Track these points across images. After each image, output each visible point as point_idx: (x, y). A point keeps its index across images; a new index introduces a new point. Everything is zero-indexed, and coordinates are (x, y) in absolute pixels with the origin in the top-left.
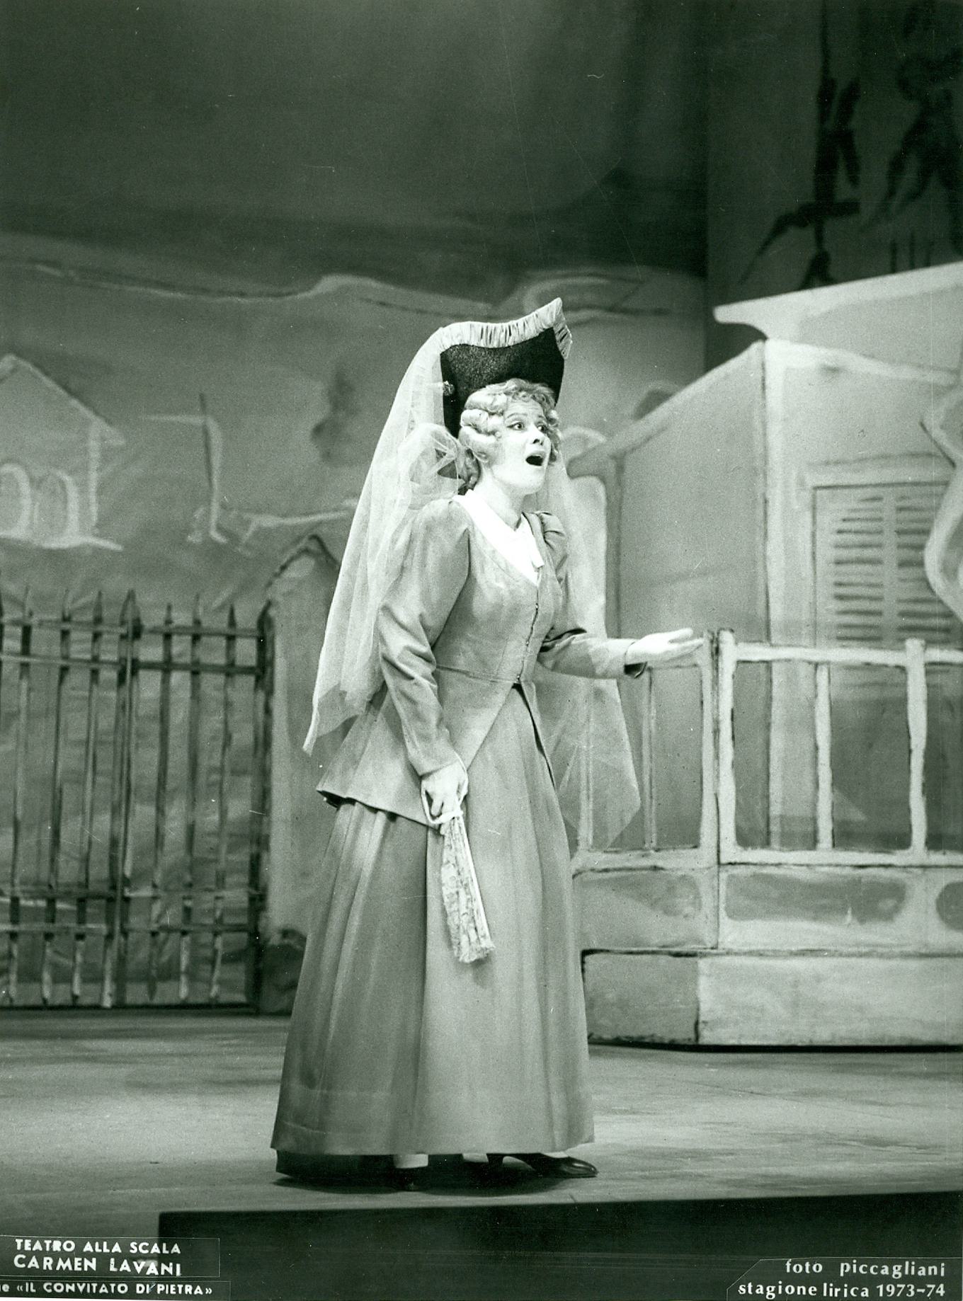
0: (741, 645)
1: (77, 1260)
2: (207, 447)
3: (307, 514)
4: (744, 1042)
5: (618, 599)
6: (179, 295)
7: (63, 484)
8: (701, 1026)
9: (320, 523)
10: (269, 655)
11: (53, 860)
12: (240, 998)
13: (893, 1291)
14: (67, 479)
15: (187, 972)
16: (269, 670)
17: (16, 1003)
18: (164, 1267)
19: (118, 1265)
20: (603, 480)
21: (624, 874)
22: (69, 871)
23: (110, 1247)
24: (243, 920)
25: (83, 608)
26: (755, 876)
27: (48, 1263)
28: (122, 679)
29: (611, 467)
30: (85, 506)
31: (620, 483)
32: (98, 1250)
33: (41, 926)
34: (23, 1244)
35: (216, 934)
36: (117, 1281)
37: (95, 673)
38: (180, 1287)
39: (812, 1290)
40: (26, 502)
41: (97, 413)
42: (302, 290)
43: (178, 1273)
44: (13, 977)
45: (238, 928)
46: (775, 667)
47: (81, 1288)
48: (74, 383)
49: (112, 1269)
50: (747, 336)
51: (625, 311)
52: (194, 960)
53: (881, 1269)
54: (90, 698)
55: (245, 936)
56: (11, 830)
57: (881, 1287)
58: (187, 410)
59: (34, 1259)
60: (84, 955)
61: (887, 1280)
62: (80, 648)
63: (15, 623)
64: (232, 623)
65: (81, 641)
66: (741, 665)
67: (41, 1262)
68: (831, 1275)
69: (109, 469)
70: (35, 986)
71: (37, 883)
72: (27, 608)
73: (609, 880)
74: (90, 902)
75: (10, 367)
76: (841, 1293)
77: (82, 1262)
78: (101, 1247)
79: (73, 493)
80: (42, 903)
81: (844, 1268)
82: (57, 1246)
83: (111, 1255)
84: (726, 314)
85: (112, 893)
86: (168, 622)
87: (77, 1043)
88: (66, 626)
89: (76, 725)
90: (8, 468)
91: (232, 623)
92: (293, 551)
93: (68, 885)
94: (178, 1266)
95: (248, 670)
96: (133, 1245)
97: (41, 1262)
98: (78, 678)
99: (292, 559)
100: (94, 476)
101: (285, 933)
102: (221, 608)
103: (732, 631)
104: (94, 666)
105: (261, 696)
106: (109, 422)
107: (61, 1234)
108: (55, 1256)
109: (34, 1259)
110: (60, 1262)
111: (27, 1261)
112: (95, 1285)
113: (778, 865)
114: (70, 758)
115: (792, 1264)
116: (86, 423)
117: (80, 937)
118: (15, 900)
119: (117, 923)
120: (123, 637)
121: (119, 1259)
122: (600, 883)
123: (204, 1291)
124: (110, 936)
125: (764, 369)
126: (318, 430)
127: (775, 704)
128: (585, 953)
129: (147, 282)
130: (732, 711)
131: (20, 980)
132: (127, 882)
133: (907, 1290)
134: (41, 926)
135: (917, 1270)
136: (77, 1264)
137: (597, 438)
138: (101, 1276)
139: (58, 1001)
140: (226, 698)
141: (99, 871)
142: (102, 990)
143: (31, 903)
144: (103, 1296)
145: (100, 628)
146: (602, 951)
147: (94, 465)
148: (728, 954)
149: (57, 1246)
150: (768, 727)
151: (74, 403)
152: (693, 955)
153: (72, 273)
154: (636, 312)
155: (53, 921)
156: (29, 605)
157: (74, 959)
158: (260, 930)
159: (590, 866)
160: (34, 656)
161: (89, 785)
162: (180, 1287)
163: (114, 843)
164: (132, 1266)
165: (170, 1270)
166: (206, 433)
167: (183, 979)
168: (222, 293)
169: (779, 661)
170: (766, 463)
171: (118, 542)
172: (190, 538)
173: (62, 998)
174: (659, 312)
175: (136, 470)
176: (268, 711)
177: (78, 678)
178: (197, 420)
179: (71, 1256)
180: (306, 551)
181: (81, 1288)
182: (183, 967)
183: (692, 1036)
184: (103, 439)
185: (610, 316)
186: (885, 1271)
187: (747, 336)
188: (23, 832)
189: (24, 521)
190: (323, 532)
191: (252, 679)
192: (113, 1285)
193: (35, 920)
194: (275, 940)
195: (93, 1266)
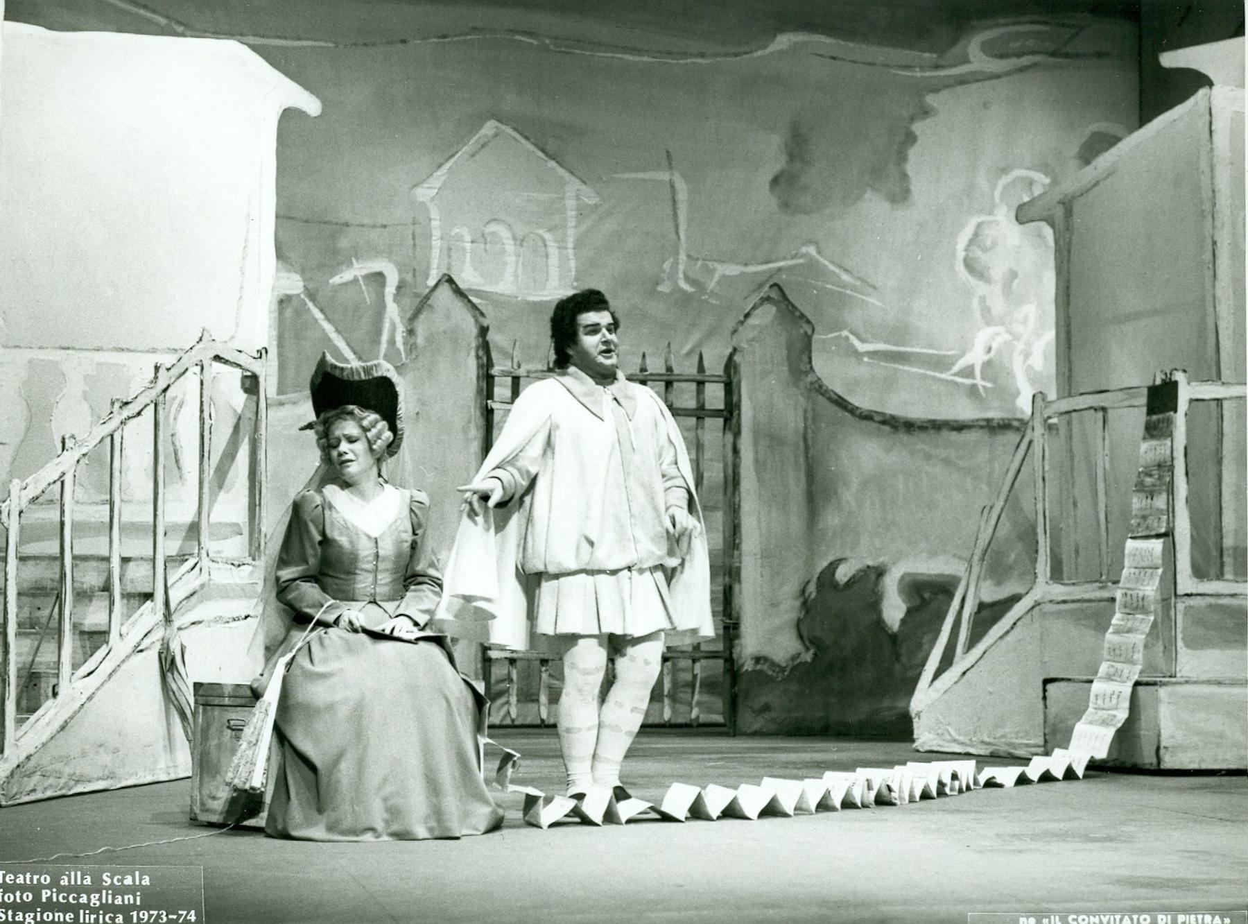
0: (1194, 384)
2: (674, 201)
3: (767, 262)
4: (1204, 767)
5: (1069, 340)
6: (645, 59)
8: (1162, 751)
9: (779, 270)
10: (735, 398)
12: (719, 719)
13: (146, 917)
14: (548, 236)
15: (669, 696)
16: (735, 414)
17: (516, 723)
20: (1052, 225)
21: (1085, 605)
24: (720, 647)
26: (1210, 606)
29: (1059, 212)
30: (563, 260)
31: (1069, 227)
35: (694, 661)
39: (69, 917)
40: (511, 259)
42: (759, 48)
44: (513, 699)
45: (713, 655)
46: (1226, 404)
48: (551, 145)
50: (1195, 81)
51: (1067, 56)
52: (675, 684)
53: (79, 897)
55: (721, 662)
57: (135, 913)
58: (657, 168)
63: (504, 374)
64: (701, 369)
66: (1194, 403)
69: (584, 227)
70: (533, 706)
72: (515, 360)
73: (1066, 611)
75: (492, 132)
76: (97, 920)
79: (553, 251)
84: (1171, 59)
86: (643, 370)
90: (492, 227)
91: (701, 369)
92: (754, 299)
95: (716, 413)
99: (754, 308)
100: (571, 234)
101: (758, 660)
102: (689, 354)
103: (1185, 371)
105: (729, 437)
113: (1233, 595)
116: (563, 183)
122: (1058, 614)
125: (1211, 114)
126: (775, 181)
127: (1226, 440)
128: (1046, 682)
129: (614, 48)
130: (1186, 449)
133: (159, 916)
135: (114, 899)
137: (1042, 179)
140: (697, 438)
146: (1063, 679)
147: (572, 223)
148: (1187, 682)
150: (1220, 461)
151: (552, 164)
152: (1155, 684)
153: (547, 41)
154: (1077, 56)
158: (735, 656)
159: (1048, 598)
166: (672, 186)
167: (666, 701)
168: (685, 55)
169: (1231, 398)
170: (1214, 205)
172: (660, 288)
174: (1100, 55)
175: (609, 226)
176: (736, 451)
178: (664, 176)
180: (767, 299)
182: (666, 693)
183: (1154, 760)
184: (578, 198)
185: (1051, 60)
186: (84, 900)
187: (1195, 81)
190: (782, 279)
191: (721, 420)
194: (749, 666)
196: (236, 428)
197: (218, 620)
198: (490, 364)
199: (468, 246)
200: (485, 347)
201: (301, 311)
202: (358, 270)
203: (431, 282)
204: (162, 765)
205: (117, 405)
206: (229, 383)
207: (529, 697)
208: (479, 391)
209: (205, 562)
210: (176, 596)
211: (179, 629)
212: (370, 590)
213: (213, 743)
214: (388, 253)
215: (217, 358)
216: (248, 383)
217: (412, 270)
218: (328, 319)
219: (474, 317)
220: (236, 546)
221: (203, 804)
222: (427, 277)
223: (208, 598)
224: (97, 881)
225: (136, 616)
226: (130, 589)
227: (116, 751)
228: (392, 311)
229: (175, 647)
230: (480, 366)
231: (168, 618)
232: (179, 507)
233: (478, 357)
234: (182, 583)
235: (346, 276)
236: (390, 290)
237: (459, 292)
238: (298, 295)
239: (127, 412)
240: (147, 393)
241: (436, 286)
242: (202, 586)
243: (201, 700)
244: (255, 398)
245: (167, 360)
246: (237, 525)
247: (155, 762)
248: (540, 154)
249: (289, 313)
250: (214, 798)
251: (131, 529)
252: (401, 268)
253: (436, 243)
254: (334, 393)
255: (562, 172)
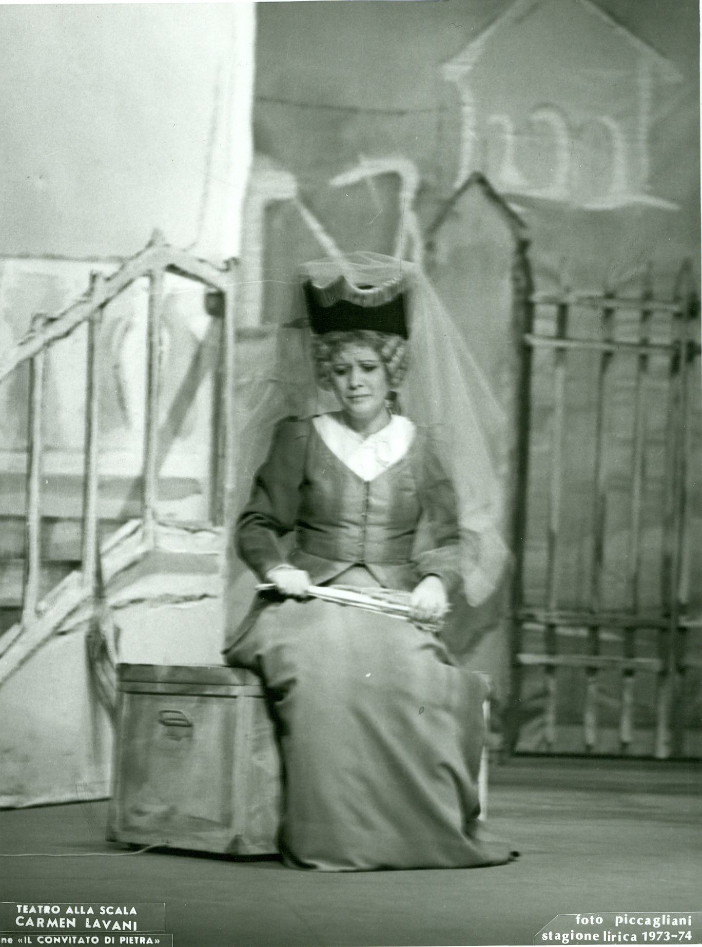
1: (61, 920)
7: (607, 135)
11: (595, 580)
14: (613, 125)
18: (124, 924)
19: (91, 923)
22: (614, 593)
23: (86, 910)
25: (631, 281)
27: (40, 922)
28: (675, 367)
32: (76, 912)
33: (581, 660)
34: (22, 908)
36: (91, 935)
37: (644, 359)
38: (136, 938)
40: (564, 155)
41: (650, 44)
43: (135, 929)
44: (550, 718)
47: (65, 940)
49: (87, 926)
54: (637, 389)
56: (545, 544)
59: (30, 920)
60: (635, 694)
61: (650, 928)
62: (626, 328)
63: (549, 301)
65: (628, 322)
67: (35, 922)
68: (608, 925)
70: (575, 730)
71: (578, 609)
74: (640, 632)
77: (65, 921)
78: (79, 910)
80: (583, 632)
81: (619, 920)
82: (47, 909)
83: (86, 916)
85: (664, 622)
87: (626, 797)
88: (610, 304)
89: (621, 418)
93: (614, 611)
94: (135, 923)
96: (102, 908)
97: (35, 922)
98: (624, 366)
100: (644, 121)
104: (643, 351)
106: (663, 54)
107: (51, 902)
108: (46, 917)
109: (30, 920)
110: (50, 922)
111: (25, 921)
112: (75, 938)
114: (614, 459)
115: (581, 917)
117: (629, 673)
118: (551, 627)
119: (672, 658)
120: (678, 316)
121: (92, 919)
123: (154, 941)
124: (663, 674)
131: (559, 722)
132: (683, 609)
134: (581, 660)
135: (671, 921)
136: (61, 923)
138: (80, 930)
139: (603, 749)
141: (650, 594)
142: (655, 736)
143: (569, 632)
144: (623, 942)
145: (650, 306)
149: (47, 909)
151: (621, 31)
155: (596, 652)
156: (566, 279)
157: (620, 698)
160: (571, 340)
161: (637, 491)
162: (136, 938)
163: (667, 562)
164: (102, 924)
165: (129, 927)
171: (673, 200)
173: (605, 742)
177: (624, 366)
179: (57, 917)
181: (65, 940)
184: (655, 75)
188: (559, 548)
189: (561, 175)
192: (88, 938)
193: (577, 652)
195: (73, 924)
196: (197, 359)
197: (166, 598)
198: (529, 288)
199: (509, 138)
200: (524, 265)
201: (293, 221)
202: (365, 170)
203: (458, 184)
204: (86, 778)
205: (40, 322)
206: (189, 298)
207: (571, 717)
208: (516, 324)
209: (151, 525)
210: (111, 565)
211: (115, 608)
212: (356, 549)
213: (140, 742)
214: (406, 147)
215: (172, 268)
216: (213, 302)
217: (435, 168)
218: (328, 231)
219: (513, 228)
220: (192, 508)
221: (125, 820)
222: (454, 176)
223: (154, 570)
224: (97, 911)
225: (58, 589)
226: (54, 556)
227: (26, 759)
228: (410, 223)
229: (107, 630)
230: (518, 291)
231: (100, 593)
232: (122, 457)
233: (515, 279)
234: (120, 551)
235: (351, 176)
236: (407, 195)
237: (493, 197)
238: (288, 201)
239: (52, 331)
240: (79, 308)
241: (465, 187)
242: (146, 555)
243: (128, 686)
244: (219, 321)
245: (108, 269)
246: (194, 481)
247: (77, 775)
248: (606, 18)
249: (278, 223)
250: (140, 813)
251: (53, 484)
252: (423, 167)
253: (469, 134)
254: (330, 318)
255: (636, 43)
